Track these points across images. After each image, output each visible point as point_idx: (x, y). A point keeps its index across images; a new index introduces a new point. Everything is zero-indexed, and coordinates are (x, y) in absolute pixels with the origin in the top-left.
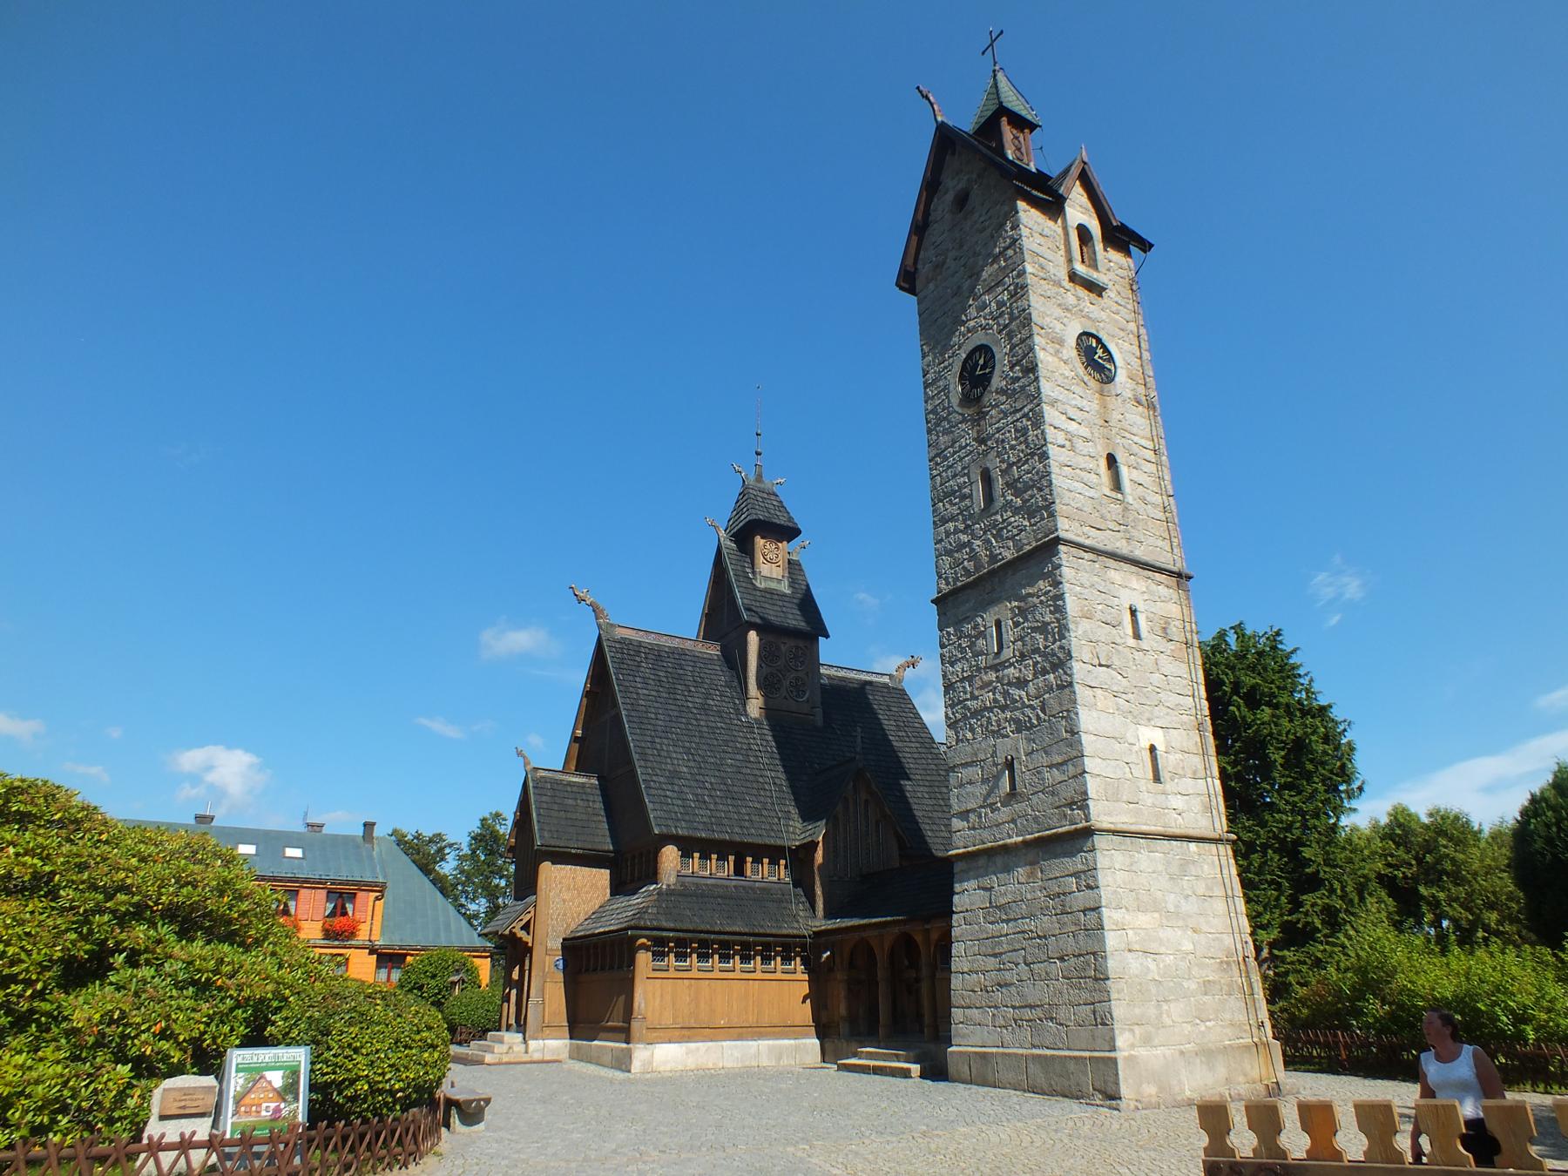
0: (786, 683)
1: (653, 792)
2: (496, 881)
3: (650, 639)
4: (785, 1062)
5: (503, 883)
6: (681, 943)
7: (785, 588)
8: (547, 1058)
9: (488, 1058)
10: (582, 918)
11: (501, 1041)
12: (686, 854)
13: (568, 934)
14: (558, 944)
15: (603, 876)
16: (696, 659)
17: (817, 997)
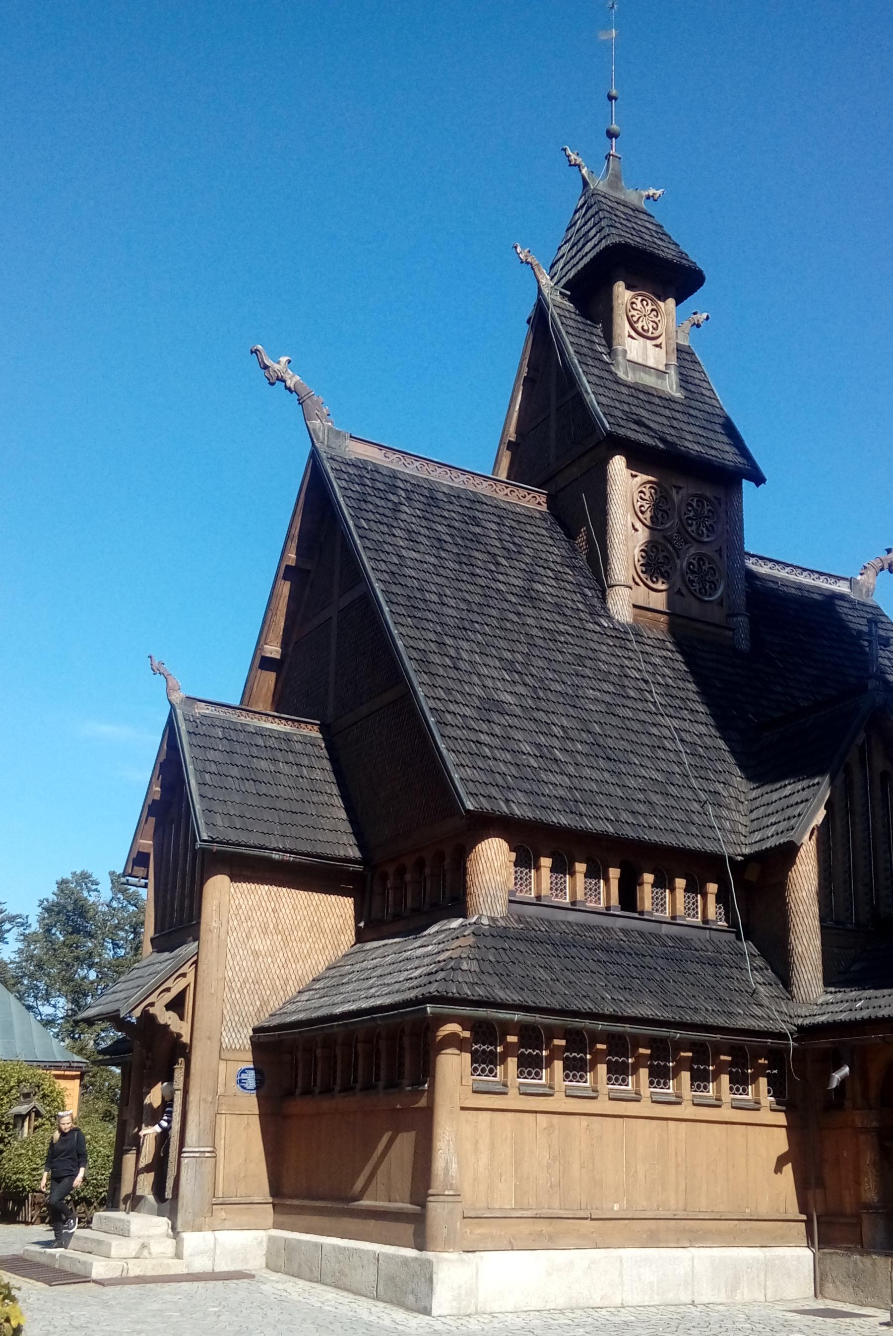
1: (449, 731)
2: (82, 973)
3: (411, 469)
4: (745, 1294)
5: (93, 975)
6: (531, 1036)
7: (670, 386)
8: (223, 1266)
9: (99, 1269)
11: (124, 1233)
12: (525, 860)
13: (263, 1020)
15: (339, 910)
16: (501, 514)
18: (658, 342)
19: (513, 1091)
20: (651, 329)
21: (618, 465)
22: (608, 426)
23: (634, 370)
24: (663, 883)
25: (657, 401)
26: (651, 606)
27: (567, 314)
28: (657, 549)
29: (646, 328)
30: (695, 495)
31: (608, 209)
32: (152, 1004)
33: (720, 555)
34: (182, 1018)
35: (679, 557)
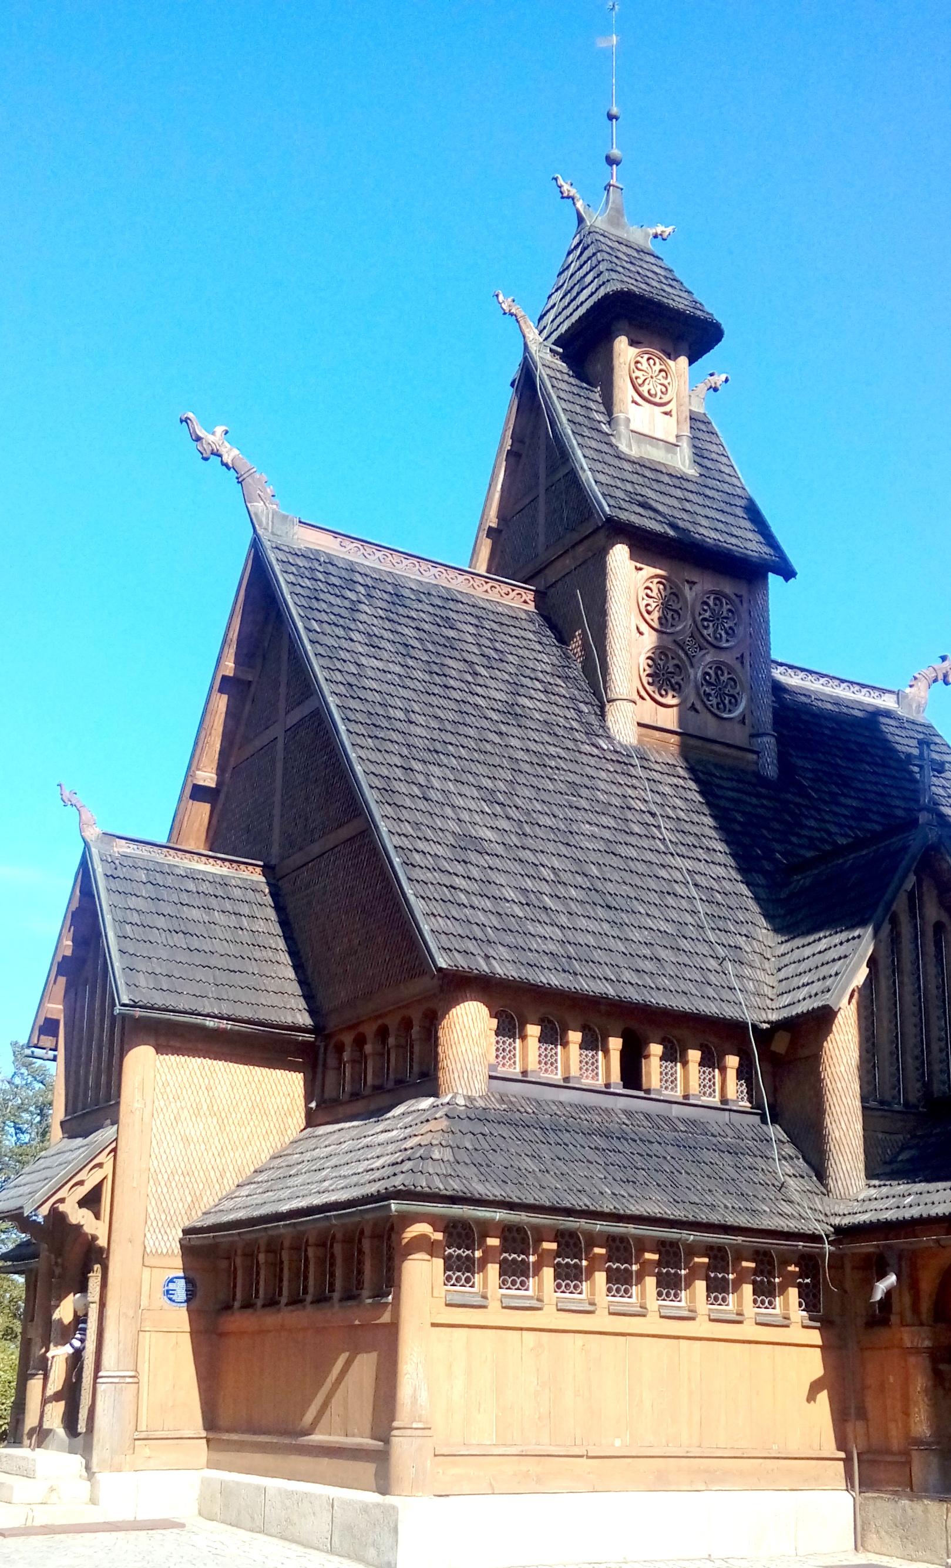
0: (696, 674)
3: (371, 561)
6: (515, 1238)
7: (682, 461)
10: (229, 1184)
12: (509, 1027)
13: (196, 1219)
14: (171, 1242)
16: (480, 614)
17: (847, 1390)
18: (667, 409)
19: (494, 1304)
20: (659, 394)
21: (619, 555)
22: (607, 509)
23: (638, 442)
24: (674, 1054)
25: (666, 479)
26: (659, 724)
27: (559, 375)
28: (666, 656)
29: (653, 392)
30: (712, 592)
31: (608, 250)
32: (62, 1200)
33: (742, 663)
34: (97, 1216)
35: (692, 666)
